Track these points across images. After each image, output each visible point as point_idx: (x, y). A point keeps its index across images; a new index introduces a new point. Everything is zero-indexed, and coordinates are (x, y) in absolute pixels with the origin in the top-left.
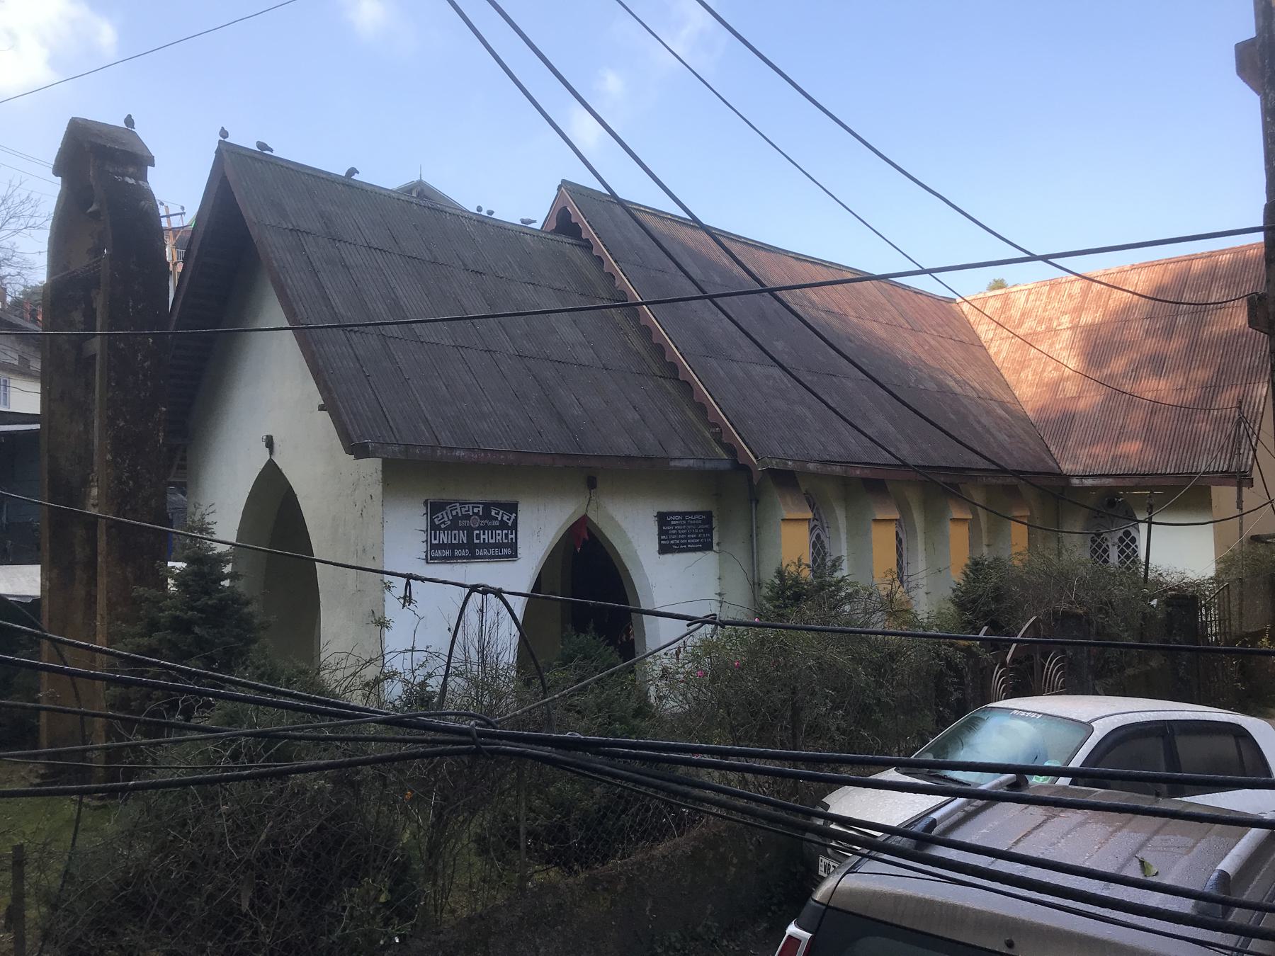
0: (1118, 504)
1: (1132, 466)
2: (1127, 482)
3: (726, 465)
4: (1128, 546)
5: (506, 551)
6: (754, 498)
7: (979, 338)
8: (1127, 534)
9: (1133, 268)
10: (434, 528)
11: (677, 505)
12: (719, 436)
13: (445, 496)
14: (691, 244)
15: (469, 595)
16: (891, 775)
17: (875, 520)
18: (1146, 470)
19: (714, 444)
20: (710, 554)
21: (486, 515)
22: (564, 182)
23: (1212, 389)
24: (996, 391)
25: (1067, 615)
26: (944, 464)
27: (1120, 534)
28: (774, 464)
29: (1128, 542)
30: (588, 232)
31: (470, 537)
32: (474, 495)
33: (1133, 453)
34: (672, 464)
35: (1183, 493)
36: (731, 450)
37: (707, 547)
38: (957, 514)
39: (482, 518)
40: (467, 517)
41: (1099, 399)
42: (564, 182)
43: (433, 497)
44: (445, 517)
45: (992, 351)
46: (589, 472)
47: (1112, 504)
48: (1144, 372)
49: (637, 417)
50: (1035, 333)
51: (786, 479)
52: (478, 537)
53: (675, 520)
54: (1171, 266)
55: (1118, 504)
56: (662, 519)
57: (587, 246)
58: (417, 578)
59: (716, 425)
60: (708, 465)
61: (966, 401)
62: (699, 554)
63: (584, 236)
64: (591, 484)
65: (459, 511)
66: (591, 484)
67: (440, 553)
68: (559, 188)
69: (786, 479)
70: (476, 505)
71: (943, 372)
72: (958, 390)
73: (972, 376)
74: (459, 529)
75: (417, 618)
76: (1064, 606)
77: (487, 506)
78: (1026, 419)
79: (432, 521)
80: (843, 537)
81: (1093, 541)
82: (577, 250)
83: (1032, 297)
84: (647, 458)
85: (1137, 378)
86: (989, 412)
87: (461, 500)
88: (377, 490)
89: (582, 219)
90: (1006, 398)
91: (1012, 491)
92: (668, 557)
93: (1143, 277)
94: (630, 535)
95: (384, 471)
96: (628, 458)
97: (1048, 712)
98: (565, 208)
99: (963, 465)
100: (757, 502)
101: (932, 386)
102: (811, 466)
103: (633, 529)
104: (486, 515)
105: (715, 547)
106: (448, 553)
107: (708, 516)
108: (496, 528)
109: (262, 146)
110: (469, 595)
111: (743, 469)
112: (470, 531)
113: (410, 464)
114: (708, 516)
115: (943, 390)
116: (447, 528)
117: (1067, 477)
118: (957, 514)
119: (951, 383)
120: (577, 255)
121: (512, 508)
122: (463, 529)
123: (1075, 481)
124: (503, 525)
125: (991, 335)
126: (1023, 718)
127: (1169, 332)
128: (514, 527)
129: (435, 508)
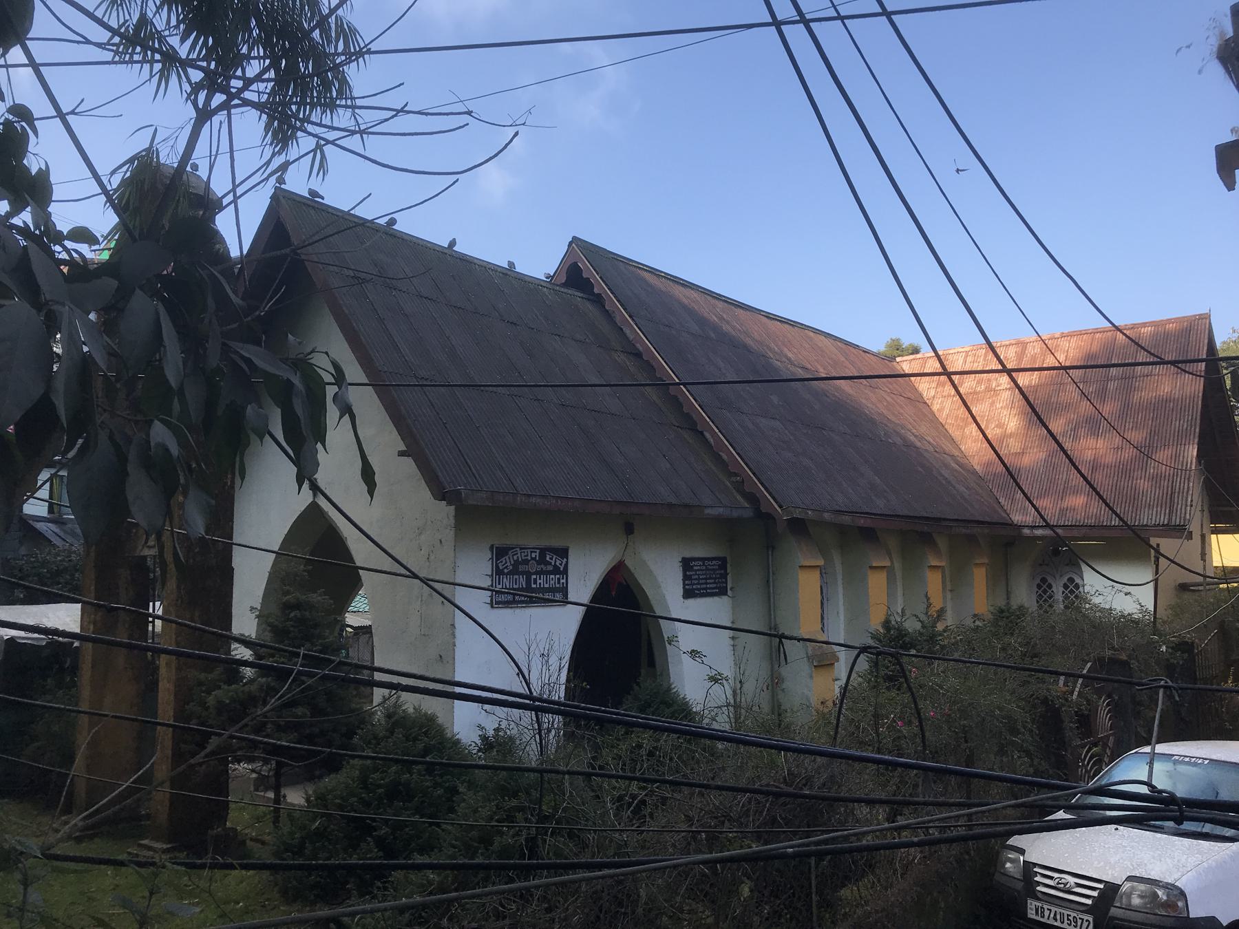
0: (1061, 552)
1: (1079, 518)
2: (1075, 533)
3: (749, 513)
4: (1072, 592)
5: (558, 596)
6: (770, 544)
7: (921, 395)
8: (1071, 580)
9: (1063, 336)
10: (499, 572)
11: (699, 551)
12: (740, 487)
13: (508, 542)
14: (686, 301)
15: (858, 656)
16: (1061, 815)
17: (871, 567)
18: (1092, 522)
19: (735, 494)
20: (725, 598)
21: (542, 560)
22: (574, 238)
23: (1145, 452)
24: (948, 447)
25: (1113, 661)
26: (905, 512)
27: (1065, 580)
28: (797, 514)
29: (1073, 587)
30: (600, 287)
31: (528, 582)
32: (531, 540)
33: (1078, 506)
34: (708, 511)
35: (1127, 542)
36: (753, 499)
37: (722, 592)
38: (934, 562)
39: (539, 563)
40: (526, 562)
41: (1042, 455)
42: (574, 238)
43: (497, 543)
44: (507, 562)
45: (935, 408)
46: (629, 520)
47: (1056, 552)
48: (1082, 432)
49: (668, 466)
50: (975, 393)
51: (799, 527)
52: (535, 582)
53: (697, 565)
54: (1097, 335)
55: (1061, 552)
56: (686, 563)
57: (598, 300)
58: (787, 638)
59: (736, 475)
60: (735, 514)
61: (926, 454)
62: (716, 599)
63: (596, 291)
64: (629, 529)
65: (520, 556)
66: (629, 529)
67: (503, 598)
68: (570, 244)
69: (799, 527)
70: (533, 549)
71: (903, 427)
72: (918, 444)
73: (923, 428)
74: (519, 573)
75: (487, 656)
76: (1108, 653)
77: (543, 551)
78: (975, 472)
79: (497, 566)
80: (840, 582)
81: (1039, 586)
82: (588, 304)
83: (969, 359)
84: (686, 506)
85: (1076, 438)
86: (947, 466)
87: (518, 544)
88: (449, 534)
89: (588, 274)
90: (956, 453)
91: (971, 539)
92: (691, 602)
93: (1073, 344)
94: (660, 580)
95: (456, 516)
96: (670, 505)
97: (1214, 757)
98: (576, 263)
99: (939, 515)
100: (773, 548)
101: (899, 441)
102: (826, 516)
103: (662, 576)
104: (542, 560)
105: (729, 592)
106: (510, 598)
107: (723, 562)
108: (550, 573)
109: (313, 193)
110: (858, 656)
111: (764, 518)
112: (528, 574)
113: (477, 507)
114: (723, 562)
115: (909, 445)
116: (510, 573)
117: (1020, 527)
118: (934, 562)
119: (912, 438)
120: (589, 307)
121: (563, 553)
122: (523, 573)
123: (1026, 531)
124: (556, 571)
125: (932, 393)
126: (1189, 763)
127: (1103, 394)
128: (565, 572)
129: (500, 553)
